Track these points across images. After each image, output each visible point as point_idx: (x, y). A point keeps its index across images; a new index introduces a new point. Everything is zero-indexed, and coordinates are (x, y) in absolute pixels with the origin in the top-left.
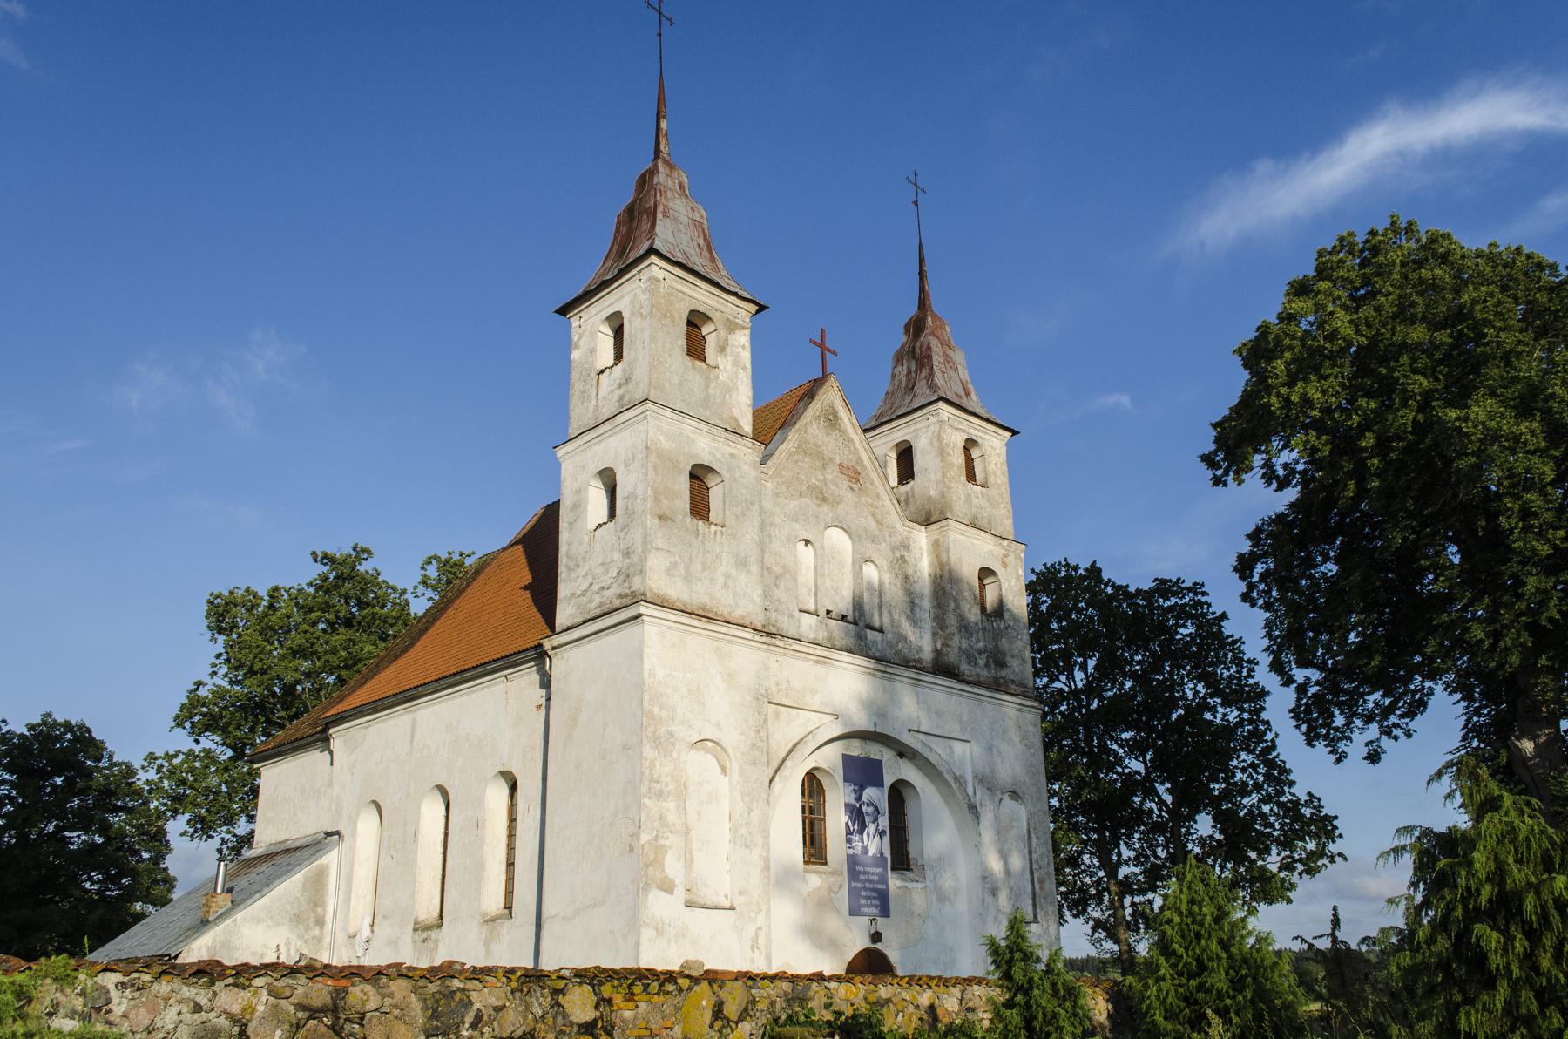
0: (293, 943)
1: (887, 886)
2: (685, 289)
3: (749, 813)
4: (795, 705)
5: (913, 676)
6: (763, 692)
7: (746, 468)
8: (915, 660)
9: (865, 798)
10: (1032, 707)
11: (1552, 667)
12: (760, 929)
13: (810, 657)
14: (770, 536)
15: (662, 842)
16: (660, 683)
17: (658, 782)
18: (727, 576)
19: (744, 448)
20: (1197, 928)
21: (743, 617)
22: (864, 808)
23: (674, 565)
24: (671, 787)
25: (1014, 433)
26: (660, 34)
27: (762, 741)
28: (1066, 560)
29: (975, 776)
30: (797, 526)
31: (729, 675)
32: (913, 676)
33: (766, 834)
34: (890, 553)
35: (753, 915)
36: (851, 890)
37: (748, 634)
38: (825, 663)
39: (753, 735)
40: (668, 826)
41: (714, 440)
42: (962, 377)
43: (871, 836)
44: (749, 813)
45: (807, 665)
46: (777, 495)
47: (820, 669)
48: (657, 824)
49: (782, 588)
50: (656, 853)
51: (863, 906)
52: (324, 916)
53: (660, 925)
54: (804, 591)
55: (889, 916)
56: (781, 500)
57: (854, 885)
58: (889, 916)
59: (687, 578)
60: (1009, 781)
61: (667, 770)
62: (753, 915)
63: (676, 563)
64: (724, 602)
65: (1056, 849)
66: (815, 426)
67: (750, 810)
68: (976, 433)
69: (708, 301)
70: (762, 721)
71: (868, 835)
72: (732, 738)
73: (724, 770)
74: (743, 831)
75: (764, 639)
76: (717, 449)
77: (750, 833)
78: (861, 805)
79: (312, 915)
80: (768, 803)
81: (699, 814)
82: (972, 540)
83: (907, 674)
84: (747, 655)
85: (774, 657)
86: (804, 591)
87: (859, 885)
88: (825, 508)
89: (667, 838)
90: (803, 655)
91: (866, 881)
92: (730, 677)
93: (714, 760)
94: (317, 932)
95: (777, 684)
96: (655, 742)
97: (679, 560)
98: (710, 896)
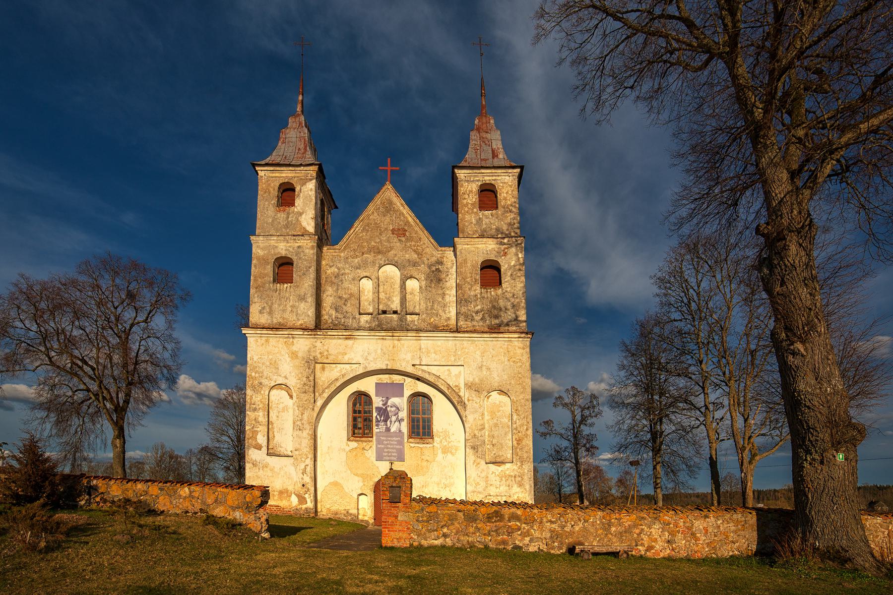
2: (277, 175)
3: (302, 415)
4: (332, 362)
5: (414, 335)
6: (312, 358)
8: (444, 326)
9: (389, 403)
10: (519, 337)
12: (308, 465)
13: (341, 337)
14: (342, 280)
16: (255, 362)
21: (301, 325)
22: (389, 409)
23: (264, 308)
24: (260, 406)
27: (310, 381)
29: (466, 384)
32: (414, 335)
34: (427, 269)
35: (303, 459)
38: (349, 338)
39: (305, 379)
40: (259, 422)
43: (393, 422)
44: (302, 415)
45: (340, 341)
47: (350, 342)
48: (253, 422)
49: (349, 305)
50: (253, 434)
51: (385, 456)
54: (366, 303)
59: (271, 313)
60: (496, 384)
61: (259, 399)
62: (303, 459)
63: (265, 307)
64: (291, 319)
65: (294, 423)
66: (376, 214)
67: (302, 414)
68: (490, 178)
69: (290, 175)
70: (310, 372)
71: (391, 422)
72: (292, 382)
73: (291, 397)
74: (299, 423)
75: (310, 333)
76: (290, 247)
77: (303, 424)
78: (386, 408)
82: (476, 246)
83: (409, 335)
84: (303, 344)
85: (319, 341)
86: (366, 303)
88: (380, 257)
90: (336, 337)
91: (387, 444)
92: (294, 355)
95: (320, 353)
97: (266, 305)
98: (282, 451)
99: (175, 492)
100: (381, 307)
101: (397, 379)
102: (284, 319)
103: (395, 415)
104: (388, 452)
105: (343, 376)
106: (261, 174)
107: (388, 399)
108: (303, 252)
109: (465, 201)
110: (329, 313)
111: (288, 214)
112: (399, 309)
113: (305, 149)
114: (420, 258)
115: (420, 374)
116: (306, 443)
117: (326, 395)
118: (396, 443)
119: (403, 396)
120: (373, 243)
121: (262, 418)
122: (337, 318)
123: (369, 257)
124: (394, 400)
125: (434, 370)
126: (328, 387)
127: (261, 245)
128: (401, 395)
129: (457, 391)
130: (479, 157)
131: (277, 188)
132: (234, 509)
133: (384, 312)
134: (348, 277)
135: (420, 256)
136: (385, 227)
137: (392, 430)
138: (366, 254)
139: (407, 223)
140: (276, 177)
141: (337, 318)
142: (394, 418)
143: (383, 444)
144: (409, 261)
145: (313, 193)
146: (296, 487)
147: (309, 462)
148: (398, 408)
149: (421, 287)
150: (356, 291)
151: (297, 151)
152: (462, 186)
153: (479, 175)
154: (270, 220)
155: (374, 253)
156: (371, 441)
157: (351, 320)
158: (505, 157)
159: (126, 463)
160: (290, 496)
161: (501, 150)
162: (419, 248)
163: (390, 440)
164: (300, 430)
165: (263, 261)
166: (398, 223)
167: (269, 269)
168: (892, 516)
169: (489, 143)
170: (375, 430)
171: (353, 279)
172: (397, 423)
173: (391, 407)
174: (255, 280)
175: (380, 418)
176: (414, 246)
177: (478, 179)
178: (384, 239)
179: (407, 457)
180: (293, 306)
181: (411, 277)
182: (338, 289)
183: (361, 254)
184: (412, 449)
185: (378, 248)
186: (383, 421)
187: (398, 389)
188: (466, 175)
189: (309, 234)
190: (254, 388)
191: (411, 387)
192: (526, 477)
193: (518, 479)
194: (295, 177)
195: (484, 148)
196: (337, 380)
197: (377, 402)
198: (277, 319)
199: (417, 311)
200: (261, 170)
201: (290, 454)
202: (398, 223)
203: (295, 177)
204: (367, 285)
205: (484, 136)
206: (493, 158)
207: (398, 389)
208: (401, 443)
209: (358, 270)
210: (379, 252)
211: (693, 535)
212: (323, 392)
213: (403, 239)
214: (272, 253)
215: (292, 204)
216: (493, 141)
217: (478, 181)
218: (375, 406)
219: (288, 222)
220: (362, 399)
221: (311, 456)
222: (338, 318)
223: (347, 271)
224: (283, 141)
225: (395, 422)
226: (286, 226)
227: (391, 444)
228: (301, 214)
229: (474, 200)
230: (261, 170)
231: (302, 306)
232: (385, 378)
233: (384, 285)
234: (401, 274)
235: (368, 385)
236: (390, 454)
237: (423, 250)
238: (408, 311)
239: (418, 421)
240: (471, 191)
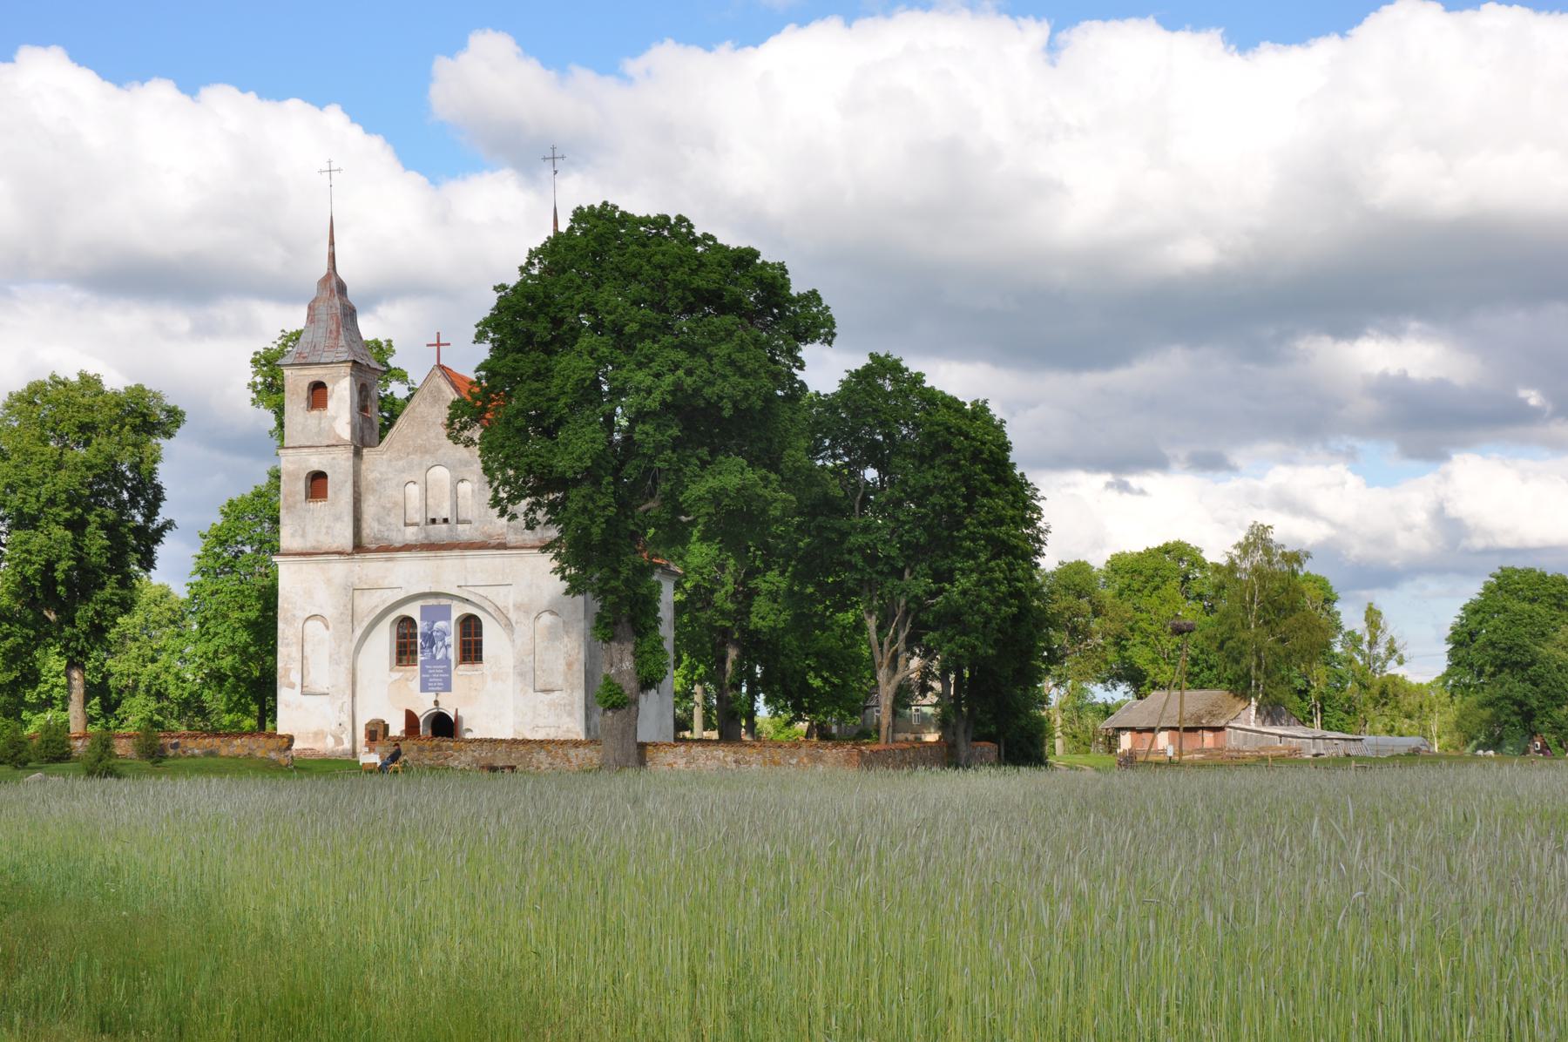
7: (343, 462)
11: (55, 582)
18: (328, 527)
20: (1204, 657)
22: (434, 634)
23: (296, 531)
28: (169, 525)
29: (514, 605)
30: (404, 475)
31: (328, 580)
36: (422, 679)
37: (336, 557)
46: (390, 461)
47: (389, 564)
49: (393, 515)
55: (450, 691)
56: (394, 463)
58: (450, 691)
59: (303, 536)
65: (330, 657)
67: (340, 646)
72: (329, 612)
73: (327, 627)
84: (340, 569)
88: (427, 457)
92: (329, 581)
98: (319, 689)
99: (231, 743)
100: (431, 516)
101: (444, 602)
102: (318, 542)
105: (384, 601)
106: (285, 371)
107: (434, 622)
110: (370, 528)
111: (320, 418)
112: (449, 516)
113: (338, 332)
115: (465, 595)
116: (344, 679)
117: (365, 624)
119: (450, 619)
120: (419, 441)
121: (296, 654)
122: (379, 531)
123: (416, 458)
124: (440, 624)
125: (481, 591)
126: (367, 616)
127: (291, 458)
128: (448, 618)
129: (505, 612)
131: (306, 389)
132: (270, 751)
133: (434, 521)
141: (379, 531)
142: (440, 644)
144: (460, 460)
145: (347, 394)
146: (333, 728)
147: (347, 698)
149: (473, 491)
150: (402, 500)
154: (300, 428)
156: (414, 671)
159: (887, 987)
160: (326, 737)
167: (301, 486)
170: (420, 657)
171: (397, 485)
172: (443, 650)
174: (285, 499)
179: (453, 686)
180: (328, 527)
181: (462, 481)
182: (380, 497)
184: (462, 674)
187: (445, 613)
191: (458, 611)
192: (576, 706)
193: (568, 708)
196: (377, 606)
197: (421, 627)
199: (469, 518)
201: (326, 691)
204: (414, 491)
207: (445, 613)
208: (448, 671)
210: (426, 452)
211: (568, 760)
212: (363, 621)
215: (324, 405)
218: (419, 631)
220: (406, 623)
221: (349, 692)
223: (390, 476)
228: (334, 418)
231: (338, 526)
232: (432, 602)
234: (451, 476)
235: (413, 611)
238: (460, 518)
239: (470, 645)
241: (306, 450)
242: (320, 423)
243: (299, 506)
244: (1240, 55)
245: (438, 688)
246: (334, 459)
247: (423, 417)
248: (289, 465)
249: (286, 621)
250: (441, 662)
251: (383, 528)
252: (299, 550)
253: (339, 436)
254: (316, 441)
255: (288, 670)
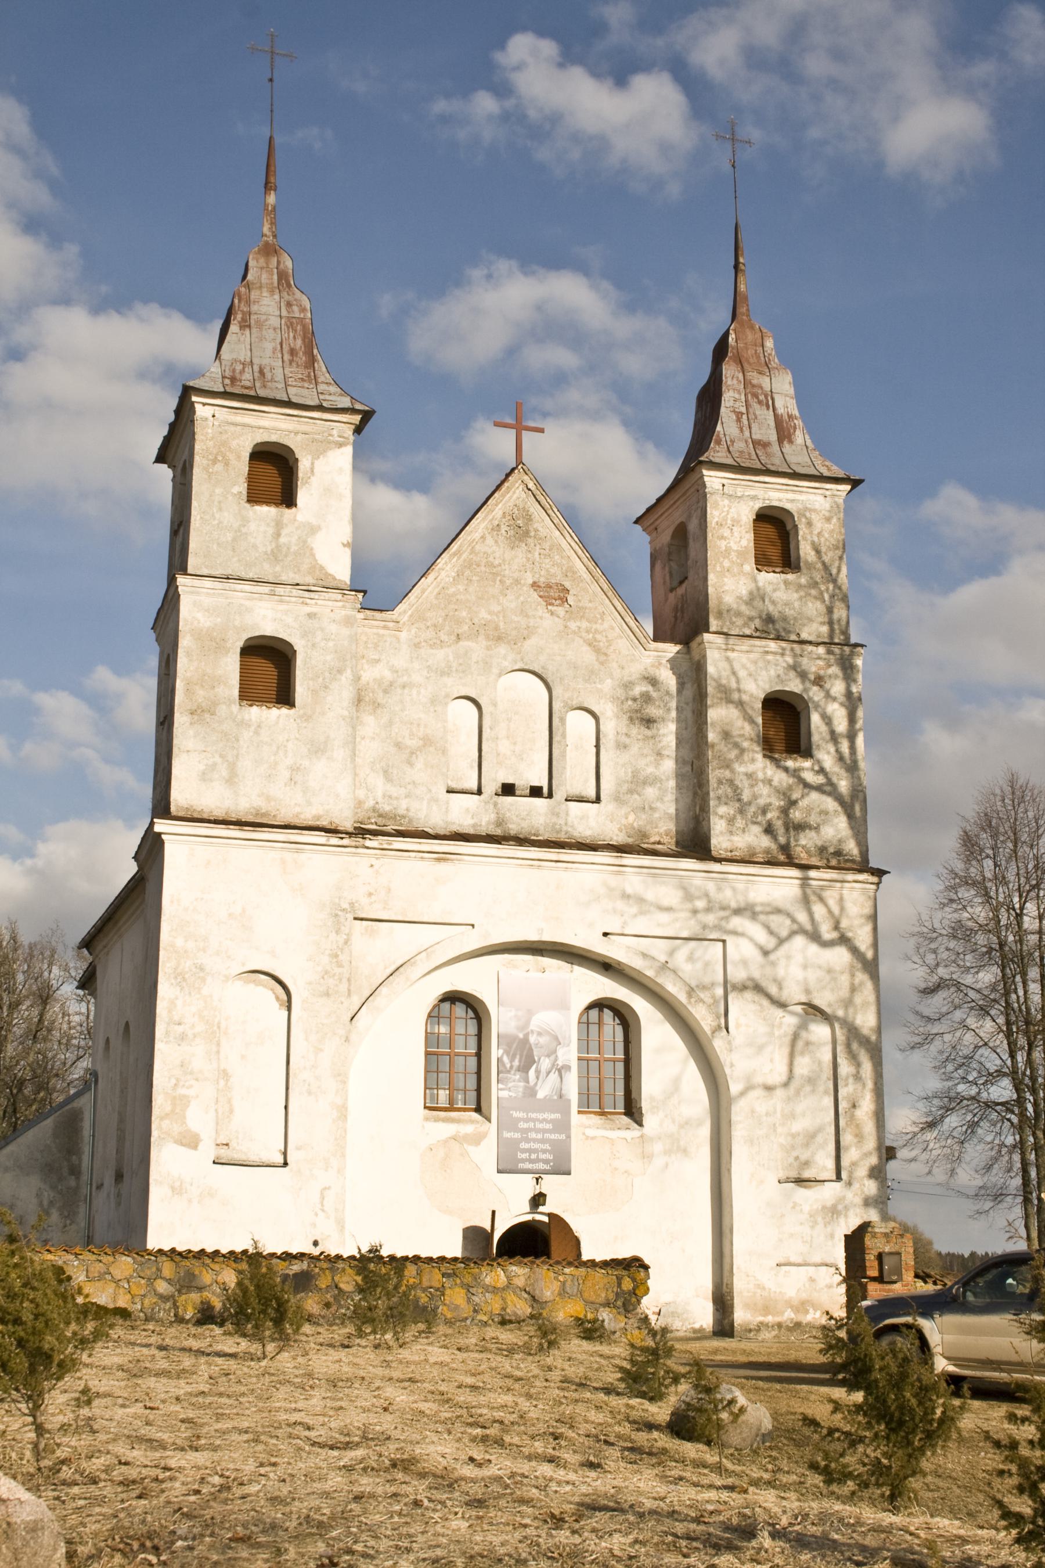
0: (46, 1194)
1: (569, 1137)
6: (345, 906)
15: (181, 1091)
17: (179, 1024)
19: (330, 603)
21: (318, 818)
22: (532, 1039)
25: (855, 483)
26: (271, 80)
30: (448, 681)
33: (341, 1078)
38: (444, 860)
40: (191, 1073)
41: (281, 601)
42: (781, 411)
46: (417, 646)
52: (80, 1165)
53: (177, 1184)
57: (507, 1135)
59: (232, 780)
63: (215, 764)
66: (490, 541)
70: (341, 941)
71: (538, 1072)
75: (346, 842)
79: (65, 1163)
80: (347, 1040)
81: (243, 1057)
87: (517, 1135)
88: (502, 649)
89: (191, 1086)
90: (412, 854)
91: (529, 1130)
93: (270, 992)
94: (72, 1183)
96: (176, 978)
102: (269, 799)
103: (548, 1056)
104: (530, 1151)
108: (322, 630)
109: (723, 544)
114: (602, 663)
118: (549, 1126)
120: (483, 615)
123: (476, 648)
130: (747, 433)
133: (508, 790)
134: (419, 693)
135: (602, 658)
136: (516, 575)
137: (540, 1095)
138: (468, 638)
139: (569, 573)
140: (244, 425)
142: (545, 1064)
143: (516, 1129)
148: (556, 1038)
151: (287, 357)
152: (716, 505)
153: (757, 484)
154: (229, 536)
155: (487, 638)
157: (425, 802)
158: (809, 443)
161: (798, 423)
162: (598, 637)
163: (534, 1120)
164: (310, 1093)
165: (211, 642)
166: (547, 571)
167: (231, 666)
168: (1044, 1550)
169: (768, 401)
172: (554, 1076)
173: (540, 1034)
175: (512, 1061)
176: (588, 632)
177: (752, 493)
178: (513, 605)
179: (576, 1164)
182: (391, 723)
183: (453, 638)
185: (497, 628)
186: (519, 1070)
188: (725, 481)
189: (331, 587)
190: (180, 977)
194: (296, 433)
195: (758, 413)
198: (242, 805)
200: (204, 404)
202: (547, 571)
203: (296, 433)
205: (755, 382)
206: (780, 441)
208: (563, 1126)
209: (445, 679)
213: (561, 611)
214: (237, 623)
216: (776, 396)
217: (754, 498)
219: (278, 547)
222: (390, 797)
223: (416, 678)
224: (244, 320)
225: (548, 1073)
226: (275, 556)
227: (538, 1131)
228: (314, 530)
229: (744, 543)
230: (204, 404)
233: (509, 720)
236: (534, 1156)
237: (610, 642)
240: (736, 522)
241: (247, 587)
242: (278, 535)
243: (222, 710)
244: (526, 274)
245: (541, 1166)
246: (311, 616)
247: (491, 565)
248: (199, 616)
249: (180, 977)
250: (546, 1105)
251: (393, 791)
252: (219, 814)
253: (322, 568)
254: (267, 571)
255: (181, 1103)
